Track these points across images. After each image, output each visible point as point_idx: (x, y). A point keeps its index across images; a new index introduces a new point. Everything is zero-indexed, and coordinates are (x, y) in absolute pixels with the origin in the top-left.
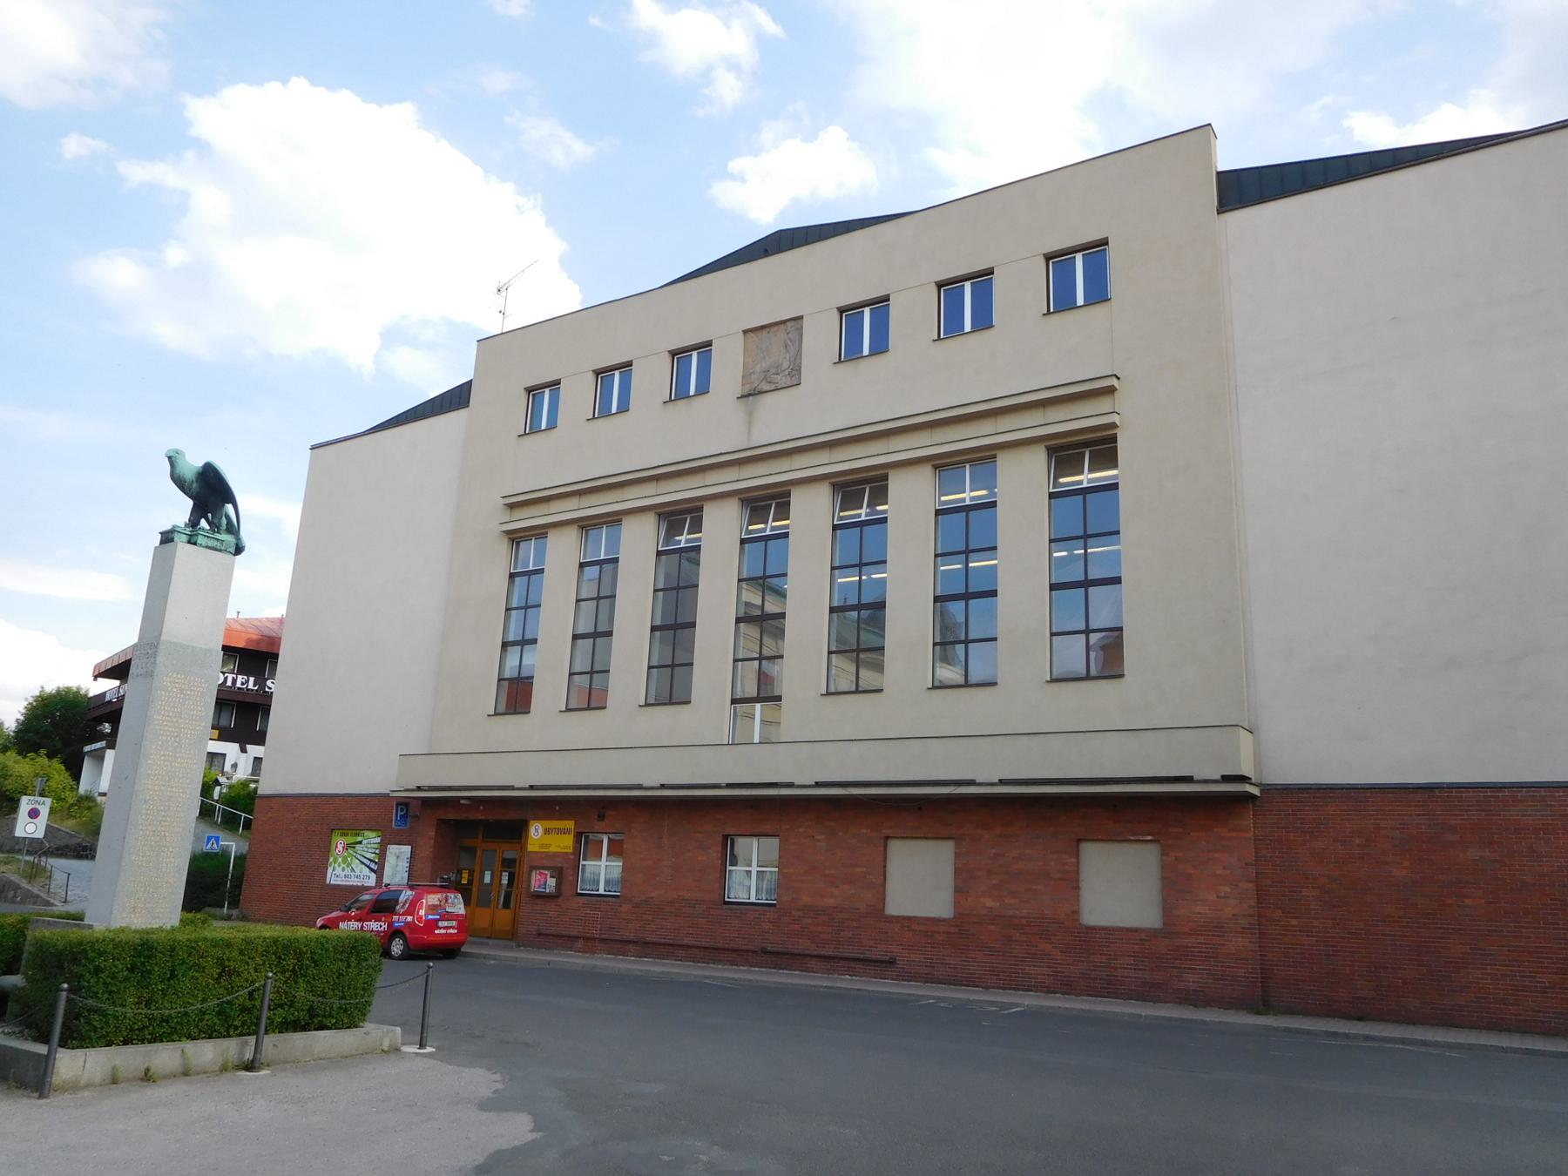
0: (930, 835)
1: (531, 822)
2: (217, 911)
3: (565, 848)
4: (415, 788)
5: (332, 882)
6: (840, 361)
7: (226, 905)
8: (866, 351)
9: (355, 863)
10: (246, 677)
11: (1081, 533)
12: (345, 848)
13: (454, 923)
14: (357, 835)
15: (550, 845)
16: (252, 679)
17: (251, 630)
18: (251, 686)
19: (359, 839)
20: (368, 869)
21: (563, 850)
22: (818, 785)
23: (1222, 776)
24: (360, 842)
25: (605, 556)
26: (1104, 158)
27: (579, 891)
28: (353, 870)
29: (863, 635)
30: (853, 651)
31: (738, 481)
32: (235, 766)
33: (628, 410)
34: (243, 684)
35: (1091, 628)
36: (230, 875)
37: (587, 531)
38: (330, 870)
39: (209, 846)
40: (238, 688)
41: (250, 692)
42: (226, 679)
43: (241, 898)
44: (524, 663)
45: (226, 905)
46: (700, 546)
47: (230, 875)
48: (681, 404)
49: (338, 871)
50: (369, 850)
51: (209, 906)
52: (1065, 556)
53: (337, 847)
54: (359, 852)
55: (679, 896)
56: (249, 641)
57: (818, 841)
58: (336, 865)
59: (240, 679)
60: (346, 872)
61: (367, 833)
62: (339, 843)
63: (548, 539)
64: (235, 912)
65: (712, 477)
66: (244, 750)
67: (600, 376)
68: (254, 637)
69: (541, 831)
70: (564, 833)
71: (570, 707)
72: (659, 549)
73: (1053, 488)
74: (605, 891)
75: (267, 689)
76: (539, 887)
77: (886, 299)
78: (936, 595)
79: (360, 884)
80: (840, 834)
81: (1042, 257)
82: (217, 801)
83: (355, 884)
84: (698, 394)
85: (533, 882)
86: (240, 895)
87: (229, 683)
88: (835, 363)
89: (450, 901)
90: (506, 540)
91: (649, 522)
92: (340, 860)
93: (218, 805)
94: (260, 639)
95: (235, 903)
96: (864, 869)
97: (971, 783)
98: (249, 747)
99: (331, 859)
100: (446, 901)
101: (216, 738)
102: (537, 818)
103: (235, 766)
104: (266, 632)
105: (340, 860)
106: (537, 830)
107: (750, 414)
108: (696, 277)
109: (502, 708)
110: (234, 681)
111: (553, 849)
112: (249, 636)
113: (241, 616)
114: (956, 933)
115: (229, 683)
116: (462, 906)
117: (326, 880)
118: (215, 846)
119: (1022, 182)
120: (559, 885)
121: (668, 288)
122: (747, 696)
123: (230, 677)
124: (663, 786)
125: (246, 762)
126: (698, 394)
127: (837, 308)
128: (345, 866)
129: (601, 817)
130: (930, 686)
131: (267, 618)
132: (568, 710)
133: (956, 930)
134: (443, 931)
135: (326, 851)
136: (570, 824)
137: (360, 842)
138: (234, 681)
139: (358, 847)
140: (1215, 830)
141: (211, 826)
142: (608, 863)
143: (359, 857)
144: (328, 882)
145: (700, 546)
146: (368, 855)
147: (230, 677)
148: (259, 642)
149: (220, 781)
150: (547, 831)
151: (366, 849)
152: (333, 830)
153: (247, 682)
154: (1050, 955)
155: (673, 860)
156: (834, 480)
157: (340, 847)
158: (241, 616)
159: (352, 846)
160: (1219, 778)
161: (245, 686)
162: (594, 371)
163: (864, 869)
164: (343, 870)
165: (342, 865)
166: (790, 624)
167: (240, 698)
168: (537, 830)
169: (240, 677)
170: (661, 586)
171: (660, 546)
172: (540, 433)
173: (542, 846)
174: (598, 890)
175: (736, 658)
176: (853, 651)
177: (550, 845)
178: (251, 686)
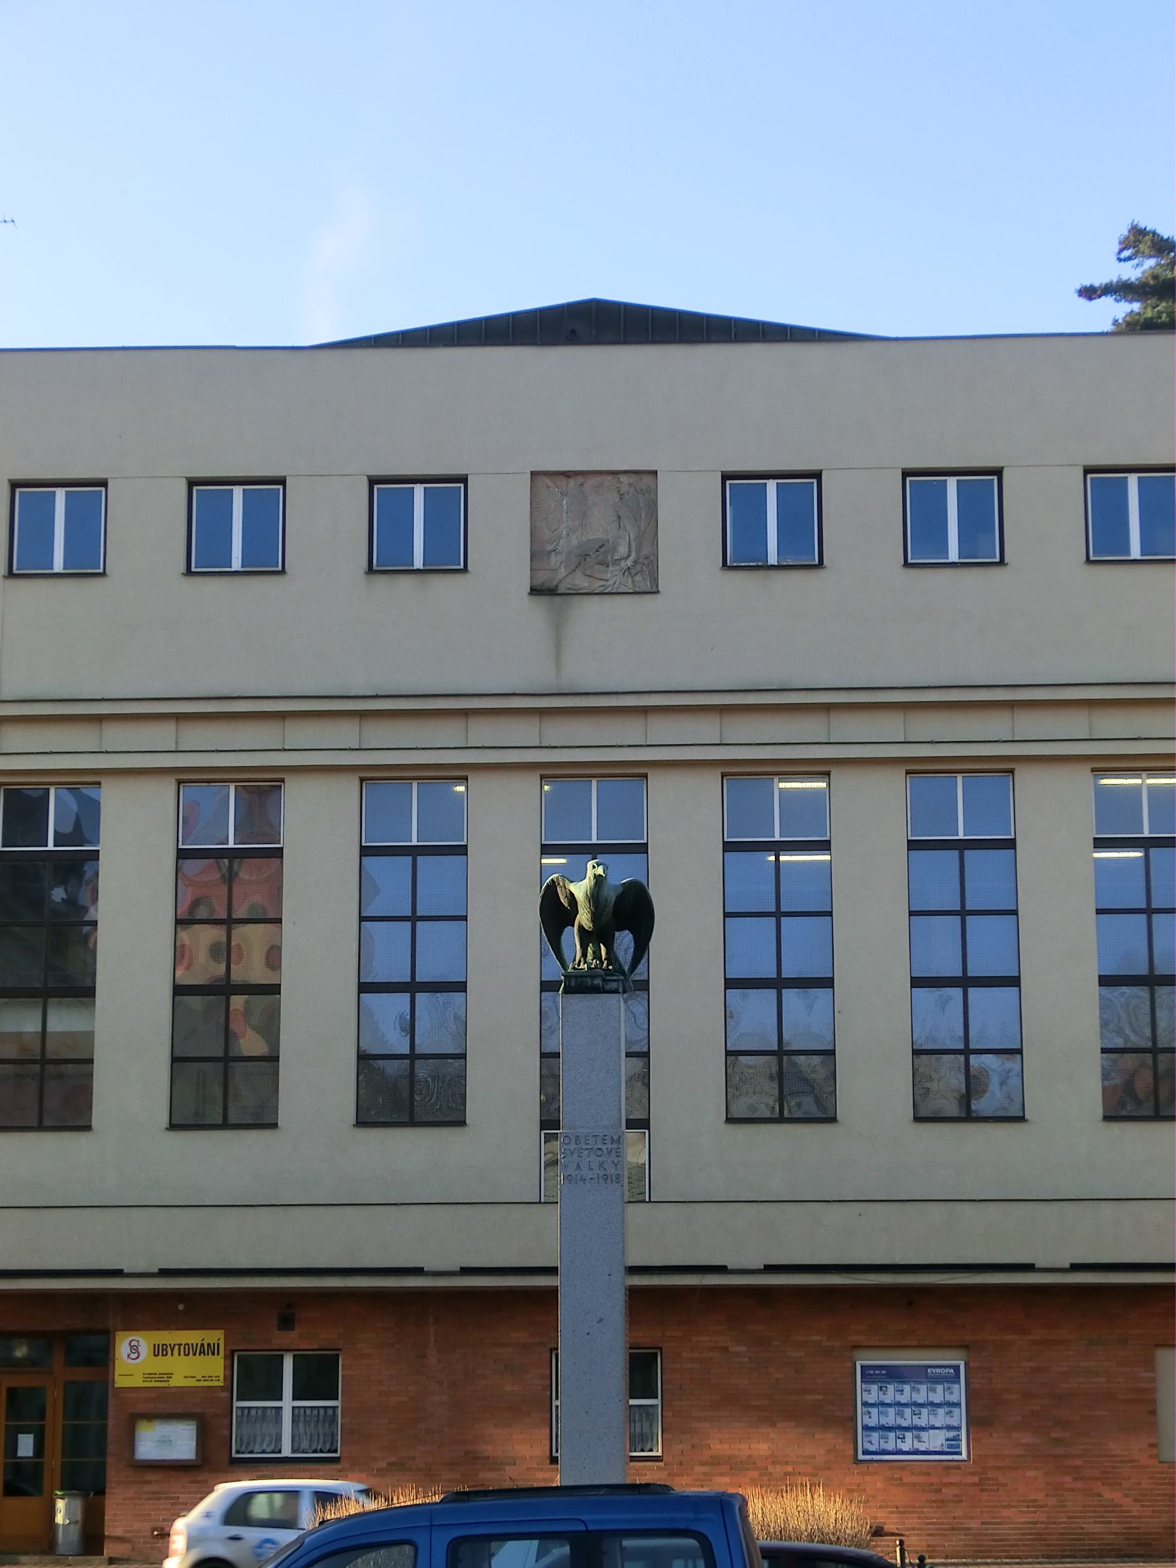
0: (927, 1343)
1: (119, 1335)
4: (156, 1270)
11: (408, 912)
21: (202, 1384)
22: (1076, 1268)
23: (461, 1268)
26: (26, 354)
27: (234, 1455)
35: (231, 1055)
44: (49, 1029)
52: (603, 944)
57: (738, 1354)
63: (102, 789)
65: (116, 736)
69: (145, 1348)
70: (202, 1352)
73: (183, 844)
74: (294, 1451)
80: (775, 1343)
81: (901, 470)
96: (821, 1397)
97: (418, 1271)
106: (134, 1349)
107: (558, 627)
111: (177, 1381)
114: (974, 1484)
119: (910, 344)
121: (1105, 339)
124: (466, 1271)
133: (976, 1479)
136: (215, 1336)
140: (694, 1339)
154: (1121, 1506)
160: (1068, 1266)
163: (821, 1397)
168: (134, 1349)
171: (180, 843)
172: (1122, 569)
173: (149, 1376)
174: (280, 1452)
176: (35, 1062)
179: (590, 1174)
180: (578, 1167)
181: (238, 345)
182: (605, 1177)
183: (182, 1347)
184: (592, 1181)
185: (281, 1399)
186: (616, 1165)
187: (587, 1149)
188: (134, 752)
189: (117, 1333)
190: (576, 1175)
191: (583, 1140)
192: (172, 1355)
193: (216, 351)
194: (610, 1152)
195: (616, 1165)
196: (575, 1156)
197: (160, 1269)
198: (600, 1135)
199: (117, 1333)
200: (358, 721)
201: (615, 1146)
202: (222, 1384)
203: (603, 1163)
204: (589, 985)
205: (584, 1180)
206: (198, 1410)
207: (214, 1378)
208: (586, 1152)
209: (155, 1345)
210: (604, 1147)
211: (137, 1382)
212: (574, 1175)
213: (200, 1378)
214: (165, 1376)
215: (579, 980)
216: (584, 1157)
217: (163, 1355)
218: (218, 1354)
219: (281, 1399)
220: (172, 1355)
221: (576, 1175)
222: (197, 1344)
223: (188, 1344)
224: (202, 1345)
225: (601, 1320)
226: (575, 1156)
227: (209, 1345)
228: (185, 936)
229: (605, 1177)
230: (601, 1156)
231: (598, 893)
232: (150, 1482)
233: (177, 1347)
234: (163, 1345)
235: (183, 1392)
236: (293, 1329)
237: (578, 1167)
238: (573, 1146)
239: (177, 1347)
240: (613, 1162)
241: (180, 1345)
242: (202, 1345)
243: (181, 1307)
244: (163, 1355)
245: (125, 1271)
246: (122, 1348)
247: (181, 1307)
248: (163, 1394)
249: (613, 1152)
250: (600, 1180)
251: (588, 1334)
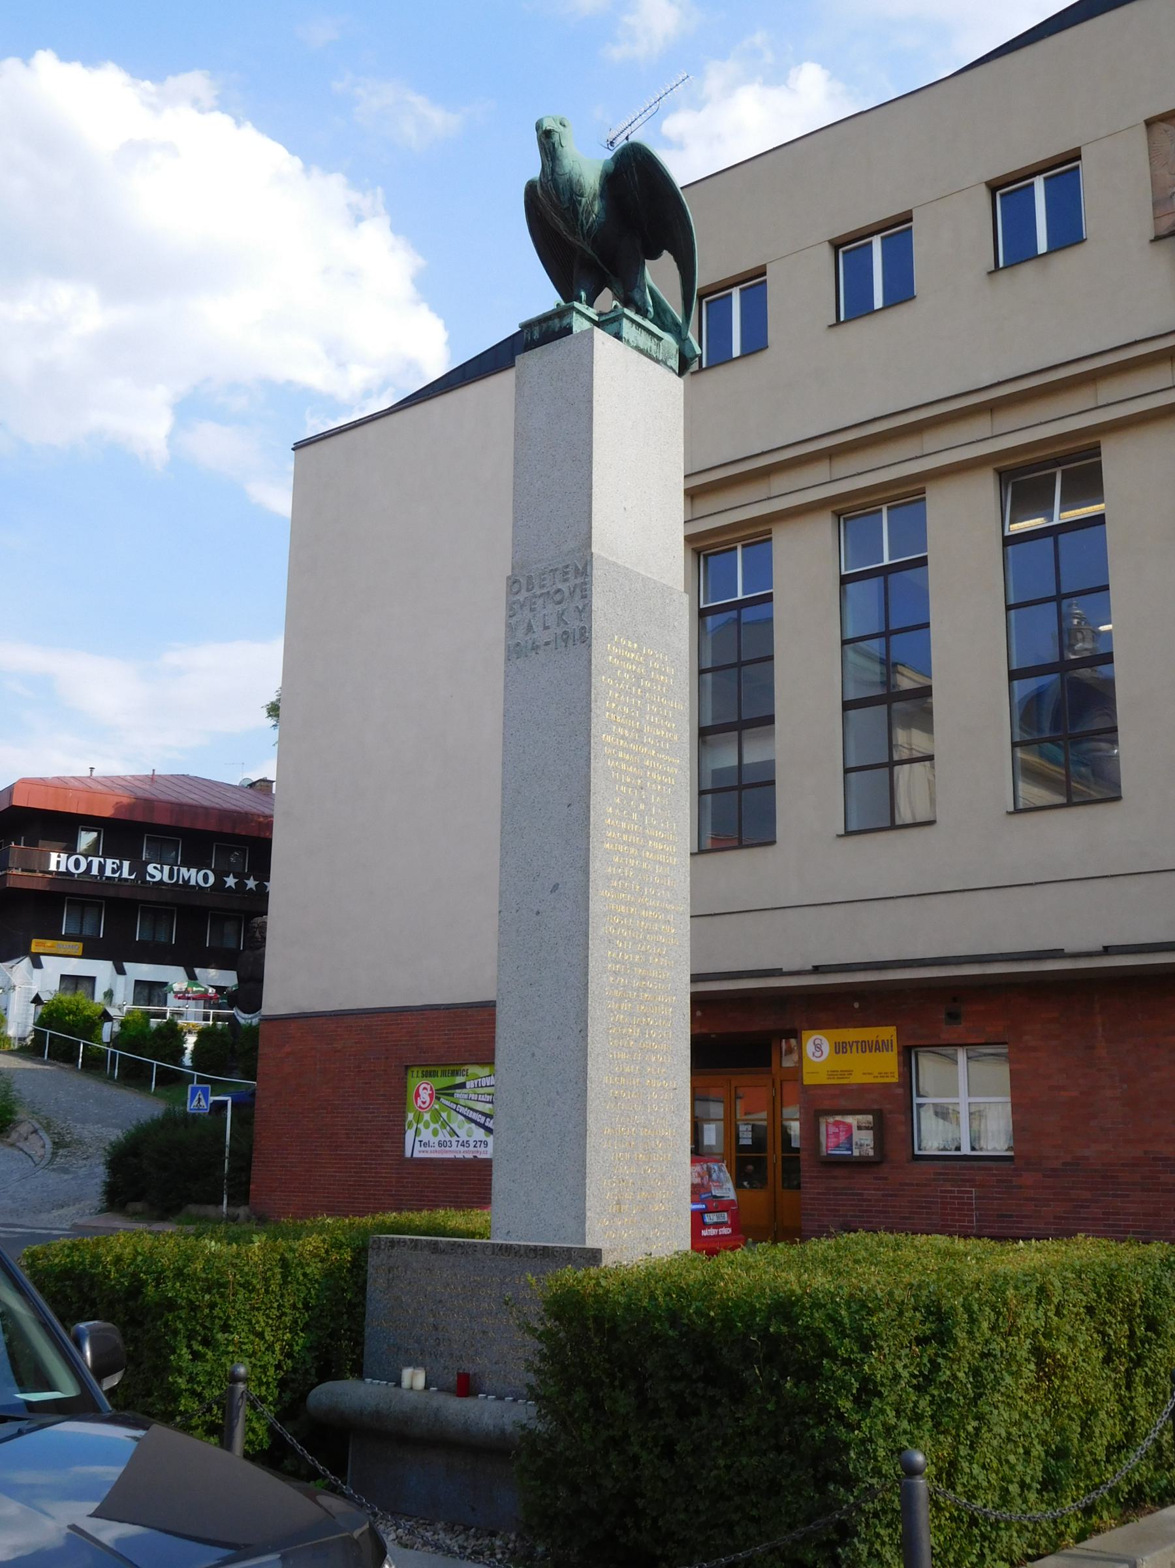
2: (210, 1210)
3: (886, 1075)
4: (810, 967)
5: (417, 1155)
6: (838, 322)
7: (225, 1202)
8: (736, 351)
9: (457, 1122)
10: (117, 861)
12: (438, 1094)
13: (725, 1217)
14: (455, 1073)
15: (850, 1072)
16: (126, 864)
17: (119, 792)
18: (125, 874)
19: (459, 1080)
20: (482, 1131)
24: (462, 1086)
25: (744, 594)
28: (453, 1133)
29: (901, 736)
30: (732, 788)
31: (769, 498)
32: (109, 994)
33: (767, 347)
34: (114, 871)
36: (227, 1150)
37: (706, 557)
38: (410, 1135)
39: (195, 1103)
40: (108, 878)
41: (123, 883)
42: (90, 865)
43: (252, 1187)
45: (225, 1202)
46: (772, 593)
47: (227, 1150)
48: (1027, 270)
49: (426, 1135)
50: (481, 1098)
51: (196, 1202)
53: (417, 1095)
54: (462, 1102)
55: (1145, 1152)
56: (119, 807)
58: (421, 1126)
59: (110, 864)
60: (440, 1137)
61: (473, 1070)
62: (422, 1088)
64: (242, 1211)
66: (121, 971)
67: (841, 250)
68: (125, 801)
69: (826, 1048)
70: (878, 1049)
71: (850, 829)
72: (702, 606)
75: (148, 878)
76: (837, 1146)
77: (761, 272)
78: (845, 699)
79: (470, 1156)
82: (108, 1044)
83: (459, 1156)
84: (745, 354)
85: (823, 1138)
86: (248, 1183)
87: (95, 871)
88: (830, 326)
89: (714, 1176)
90: (690, 550)
91: (823, 529)
92: (427, 1117)
93: (110, 1050)
94: (134, 803)
95: (241, 1196)
98: (127, 966)
99: (410, 1116)
100: (710, 1176)
101: (80, 954)
102: (815, 1026)
103: (109, 994)
104: (140, 794)
105: (427, 1117)
106: (818, 1047)
108: (972, 68)
109: (708, 844)
110: (102, 867)
111: (857, 1078)
112: (117, 799)
113: (95, 774)
115: (95, 871)
116: (730, 1185)
117: (404, 1151)
118: (203, 1103)
120: (880, 1141)
122: (918, 820)
123: (96, 861)
124: (1107, 951)
125: (125, 990)
126: (745, 354)
127: (830, 242)
128: (437, 1126)
129: (953, 1017)
130: (1011, 809)
131: (133, 776)
132: (848, 833)
134: (712, 1232)
135: (398, 1101)
136: (888, 1033)
137: (462, 1086)
138: (102, 867)
139: (458, 1093)
141: (106, 1083)
142: (972, 1100)
143: (462, 1110)
144: (408, 1154)
145: (772, 593)
146: (479, 1106)
147: (96, 861)
148: (131, 807)
149: (112, 1014)
150: (840, 1048)
151: (474, 1097)
152: (407, 1067)
153: (120, 868)
155: (1125, 1086)
156: (836, 508)
157: (425, 1096)
158: (95, 774)
159: (448, 1091)
161: (117, 875)
162: (830, 242)
164: (435, 1132)
165: (433, 1126)
166: (938, 700)
167: (111, 893)
168: (818, 1047)
169: (109, 862)
170: (708, 664)
173: (831, 1074)
175: (703, 788)
177: (850, 1072)
178: (125, 874)
179: (546, 636)
180: (530, 628)
181: (865, 110)
182: (564, 637)
183: (859, 1044)
184: (547, 647)
185: (957, 1096)
186: (580, 612)
187: (542, 594)
188: (790, 493)
189: (803, 1032)
190: (526, 642)
191: (536, 582)
192: (851, 1052)
193: (852, 120)
194: (572, 593)
195: (580, 612)
196: (526, 611)
197: (813, 967)
198: (560, 566)
199: (803, 1032)
200: (989, 418)
201: (579, 580)
202: (897, 1081)
203: (562, 614)
204: (557, 330)
205: (535, 648)
206: (875, 1107)
207: (889, 1075)
208: (540, 602)
209: (836, 1043)
210: (564, 587)
211: (822, 1079)
212: (522, 644)
213: (877, 1075)
214: (846, 1073)
215: (544, 325)
216: (538, 609)
217: (843, 1052)
218: (892, 1050)
219: (957, 1096)
220: (851, 1052)
221: (526, 642)
222: (872, 1041)
223: (845, 1043)
224: (877, 1042)
225: (556, 887)
226: (526, 611)
227: (883, 1041)
228: (921, 681)
229: (564, 637)
230: (560, 603)
231: (553, 171)
232: (834, 1178)
233: (855, 1044)
234: (843, 1043)
235: (864, 1088)
236: (960, 1024)
237: (530, 628)
238: (524, 594)
239: (855, 1044)
240: (577, 607)
241: (857, 1042)
242: (877, 1042)
243: (856, 1005)
244: (843, 1052)
245: (784, 970)
246: (808, 1045)
247: (856, 1005)
248: (844, 1091)
249: (578, 590)
250: (558, 641)
251: (538, 913)
